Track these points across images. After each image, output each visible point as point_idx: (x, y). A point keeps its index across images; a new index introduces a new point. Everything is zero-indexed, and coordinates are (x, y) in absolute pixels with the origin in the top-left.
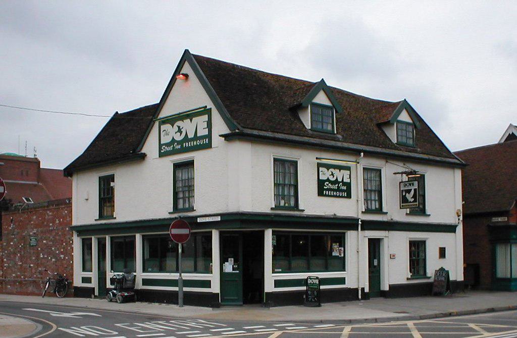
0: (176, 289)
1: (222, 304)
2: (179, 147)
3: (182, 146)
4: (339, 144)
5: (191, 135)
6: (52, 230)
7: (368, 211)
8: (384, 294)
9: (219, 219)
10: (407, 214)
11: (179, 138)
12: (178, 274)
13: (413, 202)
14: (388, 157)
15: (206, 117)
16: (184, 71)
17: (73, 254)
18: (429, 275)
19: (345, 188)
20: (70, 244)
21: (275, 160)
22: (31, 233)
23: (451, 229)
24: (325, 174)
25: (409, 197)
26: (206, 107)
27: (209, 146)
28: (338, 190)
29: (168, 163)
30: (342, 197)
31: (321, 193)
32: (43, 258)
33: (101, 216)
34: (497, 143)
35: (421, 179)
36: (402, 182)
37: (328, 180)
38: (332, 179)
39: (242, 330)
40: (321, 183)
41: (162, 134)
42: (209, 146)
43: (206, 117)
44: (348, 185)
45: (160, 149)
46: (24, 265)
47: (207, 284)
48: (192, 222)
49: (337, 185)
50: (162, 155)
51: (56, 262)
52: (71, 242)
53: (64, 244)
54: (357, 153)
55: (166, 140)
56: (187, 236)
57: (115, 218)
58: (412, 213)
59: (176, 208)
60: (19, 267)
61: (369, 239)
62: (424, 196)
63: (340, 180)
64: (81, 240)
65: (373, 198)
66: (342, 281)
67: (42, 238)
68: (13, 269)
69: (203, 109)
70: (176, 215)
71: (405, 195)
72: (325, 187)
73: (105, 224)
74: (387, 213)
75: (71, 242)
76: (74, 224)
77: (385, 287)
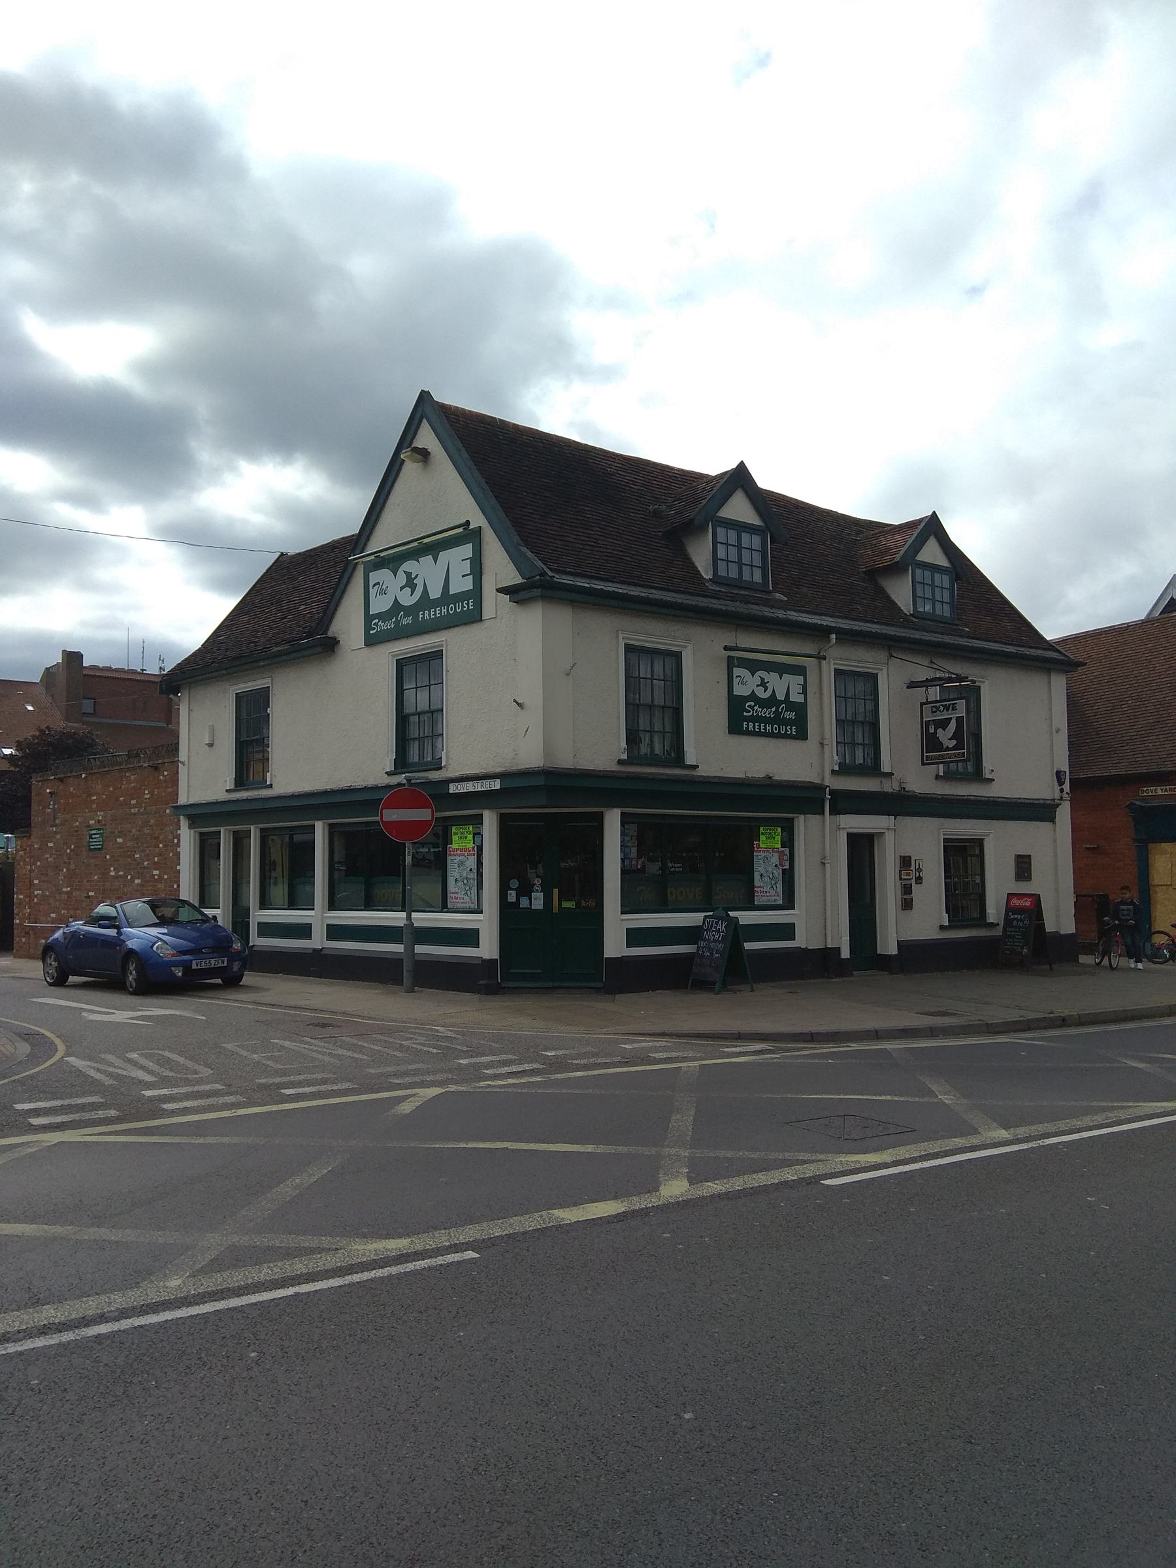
0: (399, 948)
1: (503, 985)
2: (408, 620)
3: (416, 617)
4: (781, 614)
5: (435, 593)
6: (135, 814)
7: (845, 770)
8: (884, 963)
9: (496, 785)
10: (937, 777)
11: (408, 599)
12: (403, 915)
13: (953, 749)
14: (892, 645)
15: (467, 550)
16: (419, 443)
17: (178, 868)
18: (991, 919)
19: (790, 715)
20: (173, 845)
21: (629, 649)
22: (92, 822)
23: (1042, 811)
24: (747, 684)
25: (945, 736)
26: (468, 523)
27: (475, 617)
28: (777, 720)
29: (385, 658)
30: (786, 736)
31: (736, 726)
32: (117, 877)
33: (241, 781)
34: (1142, 616)
35: (972, 694)
36: (927, 703)
37: (753, 697)
38: (761, 693)
39: (91, 1094)
40: (736, 705)
41: (372, 592)
42: (475, 617)
43: (467, 550)
44: (801, 709)
45: (368, 627)
46: (76, 894)
47: (470, 937)
48: (438, 793)
49: (774, 709)
50: (372, 641)
51: (141, 885)
52: (176, 841)
53: (161, 845)
54: (822, 633)
55: (380, 605)
56: (426, 824)
57: (271, 786)
58: (948, 777)
59: (401, 762)
60: (65, 897)
61: (849, 835)
62: (977, 737)
63: (780, 696)
64: (197, 836)
65: (658, 727)
66: (787, 931)
67: (114, 833)
68: (51, 901)
69: (461, 530)
70: (401, 778)
71: (935, 733)
72: (745, 714)
73: (247, 800)
74: (697, 767)
75: (176, 841)
76: (182, 800)
77: (888, 945)
